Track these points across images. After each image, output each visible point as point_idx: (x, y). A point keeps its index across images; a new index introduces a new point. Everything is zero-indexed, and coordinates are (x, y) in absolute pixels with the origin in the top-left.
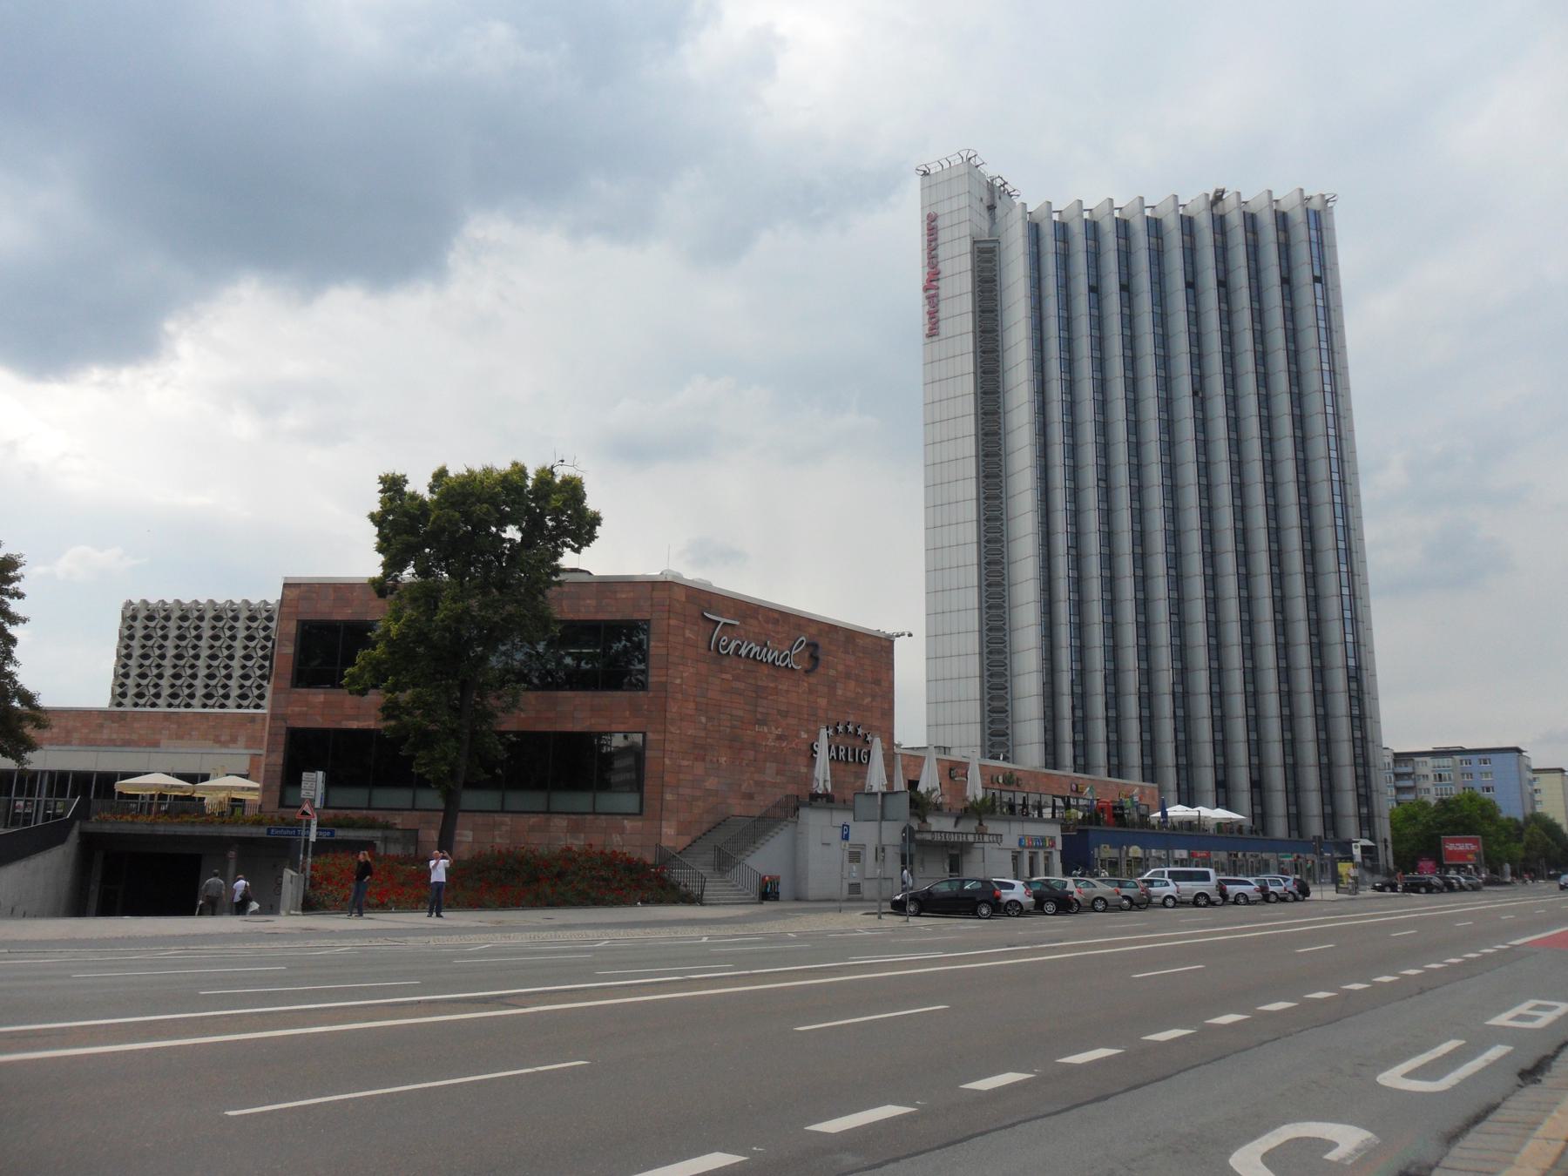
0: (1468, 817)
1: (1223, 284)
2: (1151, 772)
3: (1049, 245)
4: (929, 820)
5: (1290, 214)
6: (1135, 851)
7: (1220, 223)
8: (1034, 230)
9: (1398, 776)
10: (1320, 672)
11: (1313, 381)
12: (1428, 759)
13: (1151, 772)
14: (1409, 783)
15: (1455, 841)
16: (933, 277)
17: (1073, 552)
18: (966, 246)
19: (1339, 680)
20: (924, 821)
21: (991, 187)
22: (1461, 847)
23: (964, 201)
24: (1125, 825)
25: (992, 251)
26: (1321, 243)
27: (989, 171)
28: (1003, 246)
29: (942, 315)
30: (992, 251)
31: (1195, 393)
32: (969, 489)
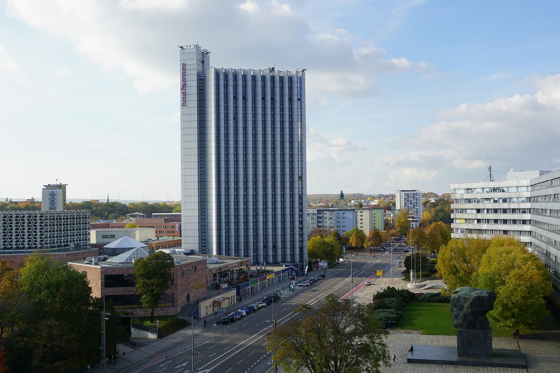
1: (273, 99)
3: (222, 77)
7: (273, 78)
10: (292, 196)
11: (296, 158)
16: (184, 86)
18: (195, 78)
19: (297, 198)
23: (195, 62)
28: (207, 79)
29: (187, 99)
30: (203, 80)
32: (195, 158)
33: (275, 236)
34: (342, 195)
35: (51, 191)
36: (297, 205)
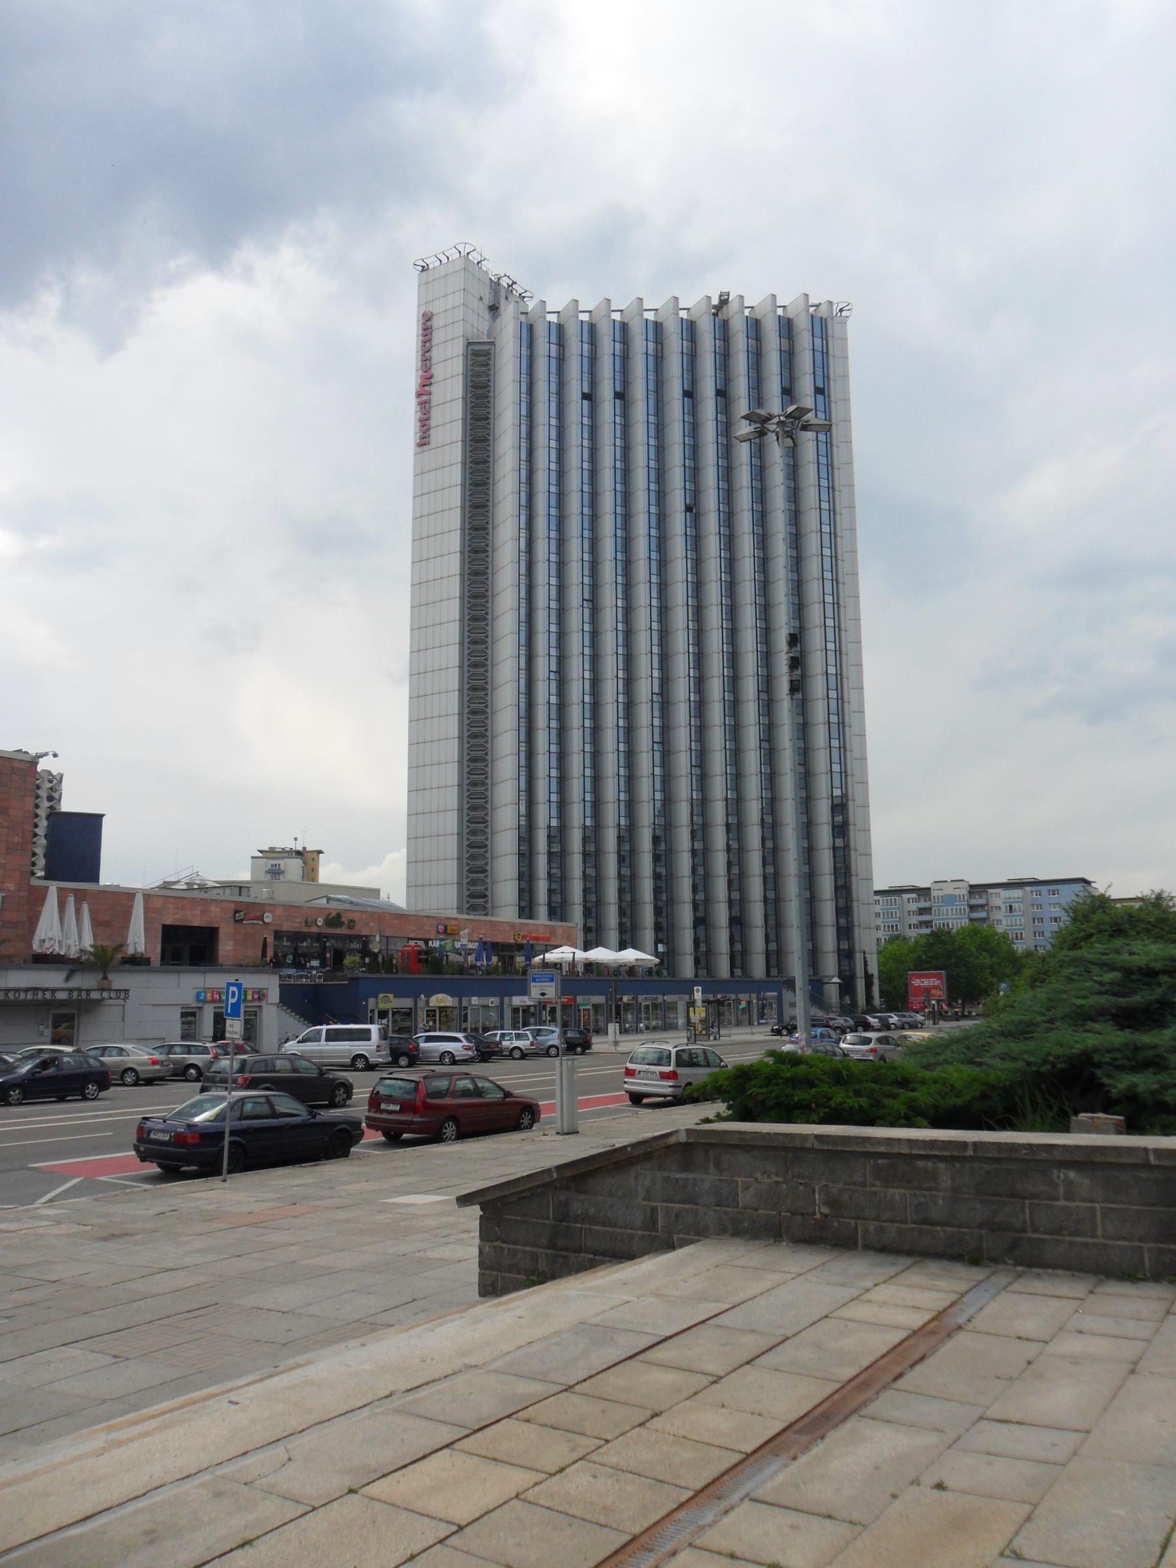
0: (961, 948)
2: (558, 911)
3: (544, 348)
4: (111, 976)
5: (795, 320)
6: (441, 1000)
8: (529, 333)
9: (973, 908)
10: (807, 803)
12: (999, 890)
13: (558, 911)
14: (983, 915)
15: (921, 977)
16: (426, 382)
17: (764, 696)
18: (458, 348)
20: (105, 978)
21: (495, 285)
22: (926, 983)
24: (439, 972)
25: (487, 354)
26: (825, 353)
27: (493, 268)
28: (498, 350)
31: (688, 509)
33: (737, 882)
34: (877, 1468)
35: (274, 862)
36: (824, 835)
